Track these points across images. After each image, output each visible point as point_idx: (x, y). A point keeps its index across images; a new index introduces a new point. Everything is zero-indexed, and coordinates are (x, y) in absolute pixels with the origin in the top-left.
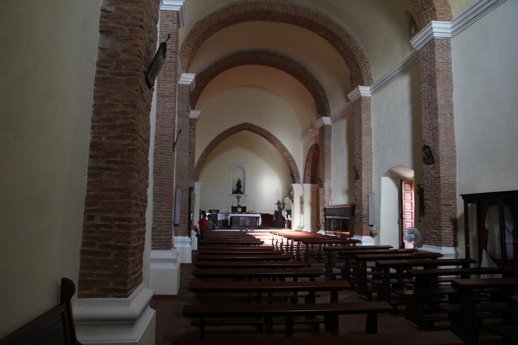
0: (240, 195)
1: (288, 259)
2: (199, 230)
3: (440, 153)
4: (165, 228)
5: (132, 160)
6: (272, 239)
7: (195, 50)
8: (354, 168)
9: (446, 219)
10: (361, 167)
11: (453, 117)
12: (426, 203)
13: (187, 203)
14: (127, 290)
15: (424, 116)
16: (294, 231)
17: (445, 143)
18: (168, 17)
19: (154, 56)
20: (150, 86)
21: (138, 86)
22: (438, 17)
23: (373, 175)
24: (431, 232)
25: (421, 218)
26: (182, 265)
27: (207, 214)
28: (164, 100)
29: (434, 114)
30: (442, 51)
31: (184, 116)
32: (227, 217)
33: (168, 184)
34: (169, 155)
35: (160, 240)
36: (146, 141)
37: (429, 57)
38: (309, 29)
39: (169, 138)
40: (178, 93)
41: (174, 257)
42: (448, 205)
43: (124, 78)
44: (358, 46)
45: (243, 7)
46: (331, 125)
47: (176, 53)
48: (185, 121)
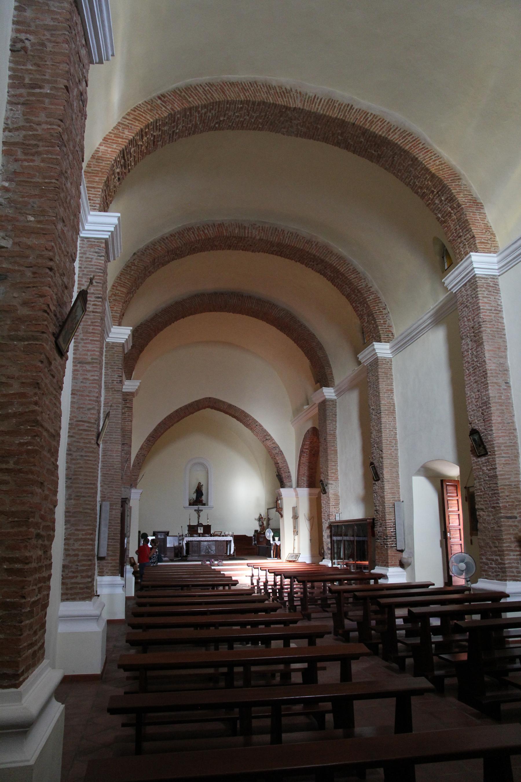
0: (201, 507)
1: (274, 609)
2: (138, 564)
3: (495, 441)
4: (83, 565)
5: (32, 467)
6: (251, 575)
7: (132, 292)
8: (372, 464)
9: (510, 538)
10: (382, 462)
11: (510, 387)
12: (479, 515)
13: (118, 523)
14: (18, 675)
15: (469, 385)
16: (284, 561)
17: (500, 426)
18: (92, 247)
19: (69, 309)
20: (62, 354)
21: (43, 356)
22: (478, 247)
23: (400, 473)
24: (489, 560)
25: (474, 538)
26: (110, 622)
27: (150, 538)
28: (84, 368)
29: (482, 383)
30: (487, 294)
31: (115, 391)
32: (181, 542)
33: (89, 496)
34: (91, 452)
35: (75, 586)
36: (54, 436)
37: (470, 303)
38: (299, 261)
39: (90, 425)
40: (105, 355)
41: (97, 612)
42: (511, 518)
43: (22, 343)
44: (370, 285)
45: (203, 231)
46: (336, 400)
47: (103, 299)
48: (117, 397)
